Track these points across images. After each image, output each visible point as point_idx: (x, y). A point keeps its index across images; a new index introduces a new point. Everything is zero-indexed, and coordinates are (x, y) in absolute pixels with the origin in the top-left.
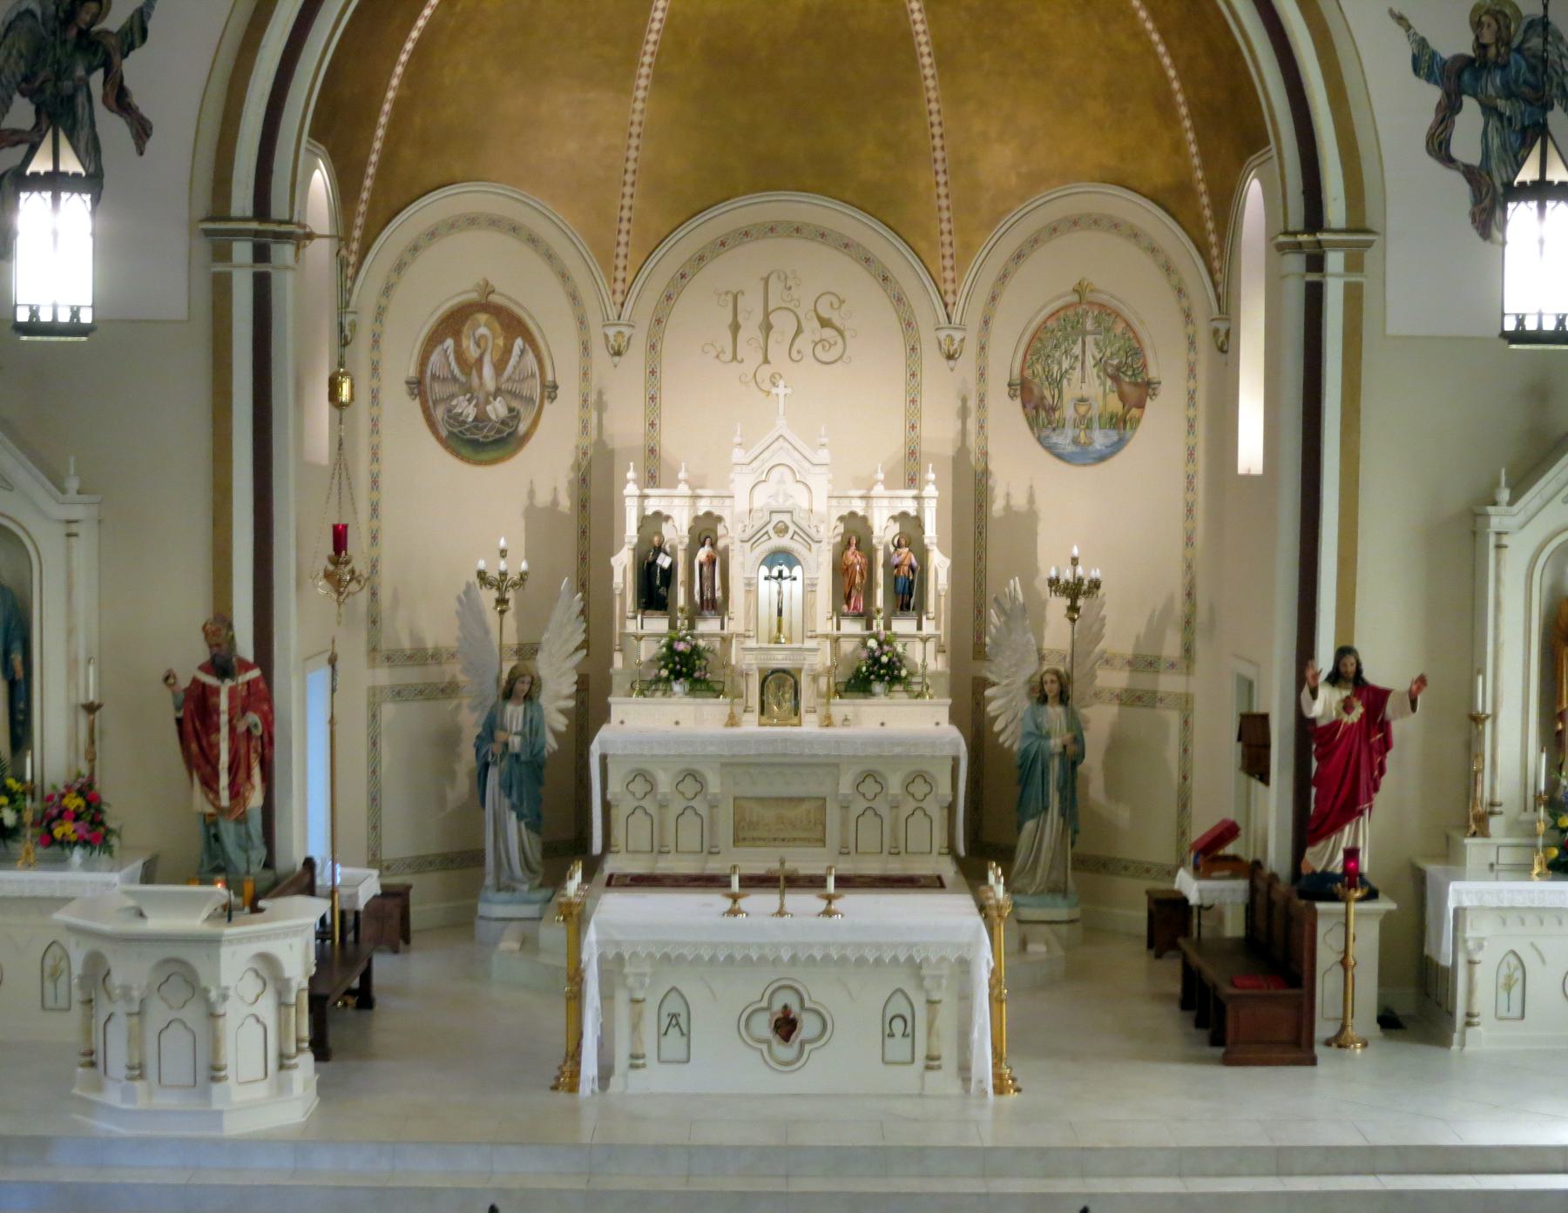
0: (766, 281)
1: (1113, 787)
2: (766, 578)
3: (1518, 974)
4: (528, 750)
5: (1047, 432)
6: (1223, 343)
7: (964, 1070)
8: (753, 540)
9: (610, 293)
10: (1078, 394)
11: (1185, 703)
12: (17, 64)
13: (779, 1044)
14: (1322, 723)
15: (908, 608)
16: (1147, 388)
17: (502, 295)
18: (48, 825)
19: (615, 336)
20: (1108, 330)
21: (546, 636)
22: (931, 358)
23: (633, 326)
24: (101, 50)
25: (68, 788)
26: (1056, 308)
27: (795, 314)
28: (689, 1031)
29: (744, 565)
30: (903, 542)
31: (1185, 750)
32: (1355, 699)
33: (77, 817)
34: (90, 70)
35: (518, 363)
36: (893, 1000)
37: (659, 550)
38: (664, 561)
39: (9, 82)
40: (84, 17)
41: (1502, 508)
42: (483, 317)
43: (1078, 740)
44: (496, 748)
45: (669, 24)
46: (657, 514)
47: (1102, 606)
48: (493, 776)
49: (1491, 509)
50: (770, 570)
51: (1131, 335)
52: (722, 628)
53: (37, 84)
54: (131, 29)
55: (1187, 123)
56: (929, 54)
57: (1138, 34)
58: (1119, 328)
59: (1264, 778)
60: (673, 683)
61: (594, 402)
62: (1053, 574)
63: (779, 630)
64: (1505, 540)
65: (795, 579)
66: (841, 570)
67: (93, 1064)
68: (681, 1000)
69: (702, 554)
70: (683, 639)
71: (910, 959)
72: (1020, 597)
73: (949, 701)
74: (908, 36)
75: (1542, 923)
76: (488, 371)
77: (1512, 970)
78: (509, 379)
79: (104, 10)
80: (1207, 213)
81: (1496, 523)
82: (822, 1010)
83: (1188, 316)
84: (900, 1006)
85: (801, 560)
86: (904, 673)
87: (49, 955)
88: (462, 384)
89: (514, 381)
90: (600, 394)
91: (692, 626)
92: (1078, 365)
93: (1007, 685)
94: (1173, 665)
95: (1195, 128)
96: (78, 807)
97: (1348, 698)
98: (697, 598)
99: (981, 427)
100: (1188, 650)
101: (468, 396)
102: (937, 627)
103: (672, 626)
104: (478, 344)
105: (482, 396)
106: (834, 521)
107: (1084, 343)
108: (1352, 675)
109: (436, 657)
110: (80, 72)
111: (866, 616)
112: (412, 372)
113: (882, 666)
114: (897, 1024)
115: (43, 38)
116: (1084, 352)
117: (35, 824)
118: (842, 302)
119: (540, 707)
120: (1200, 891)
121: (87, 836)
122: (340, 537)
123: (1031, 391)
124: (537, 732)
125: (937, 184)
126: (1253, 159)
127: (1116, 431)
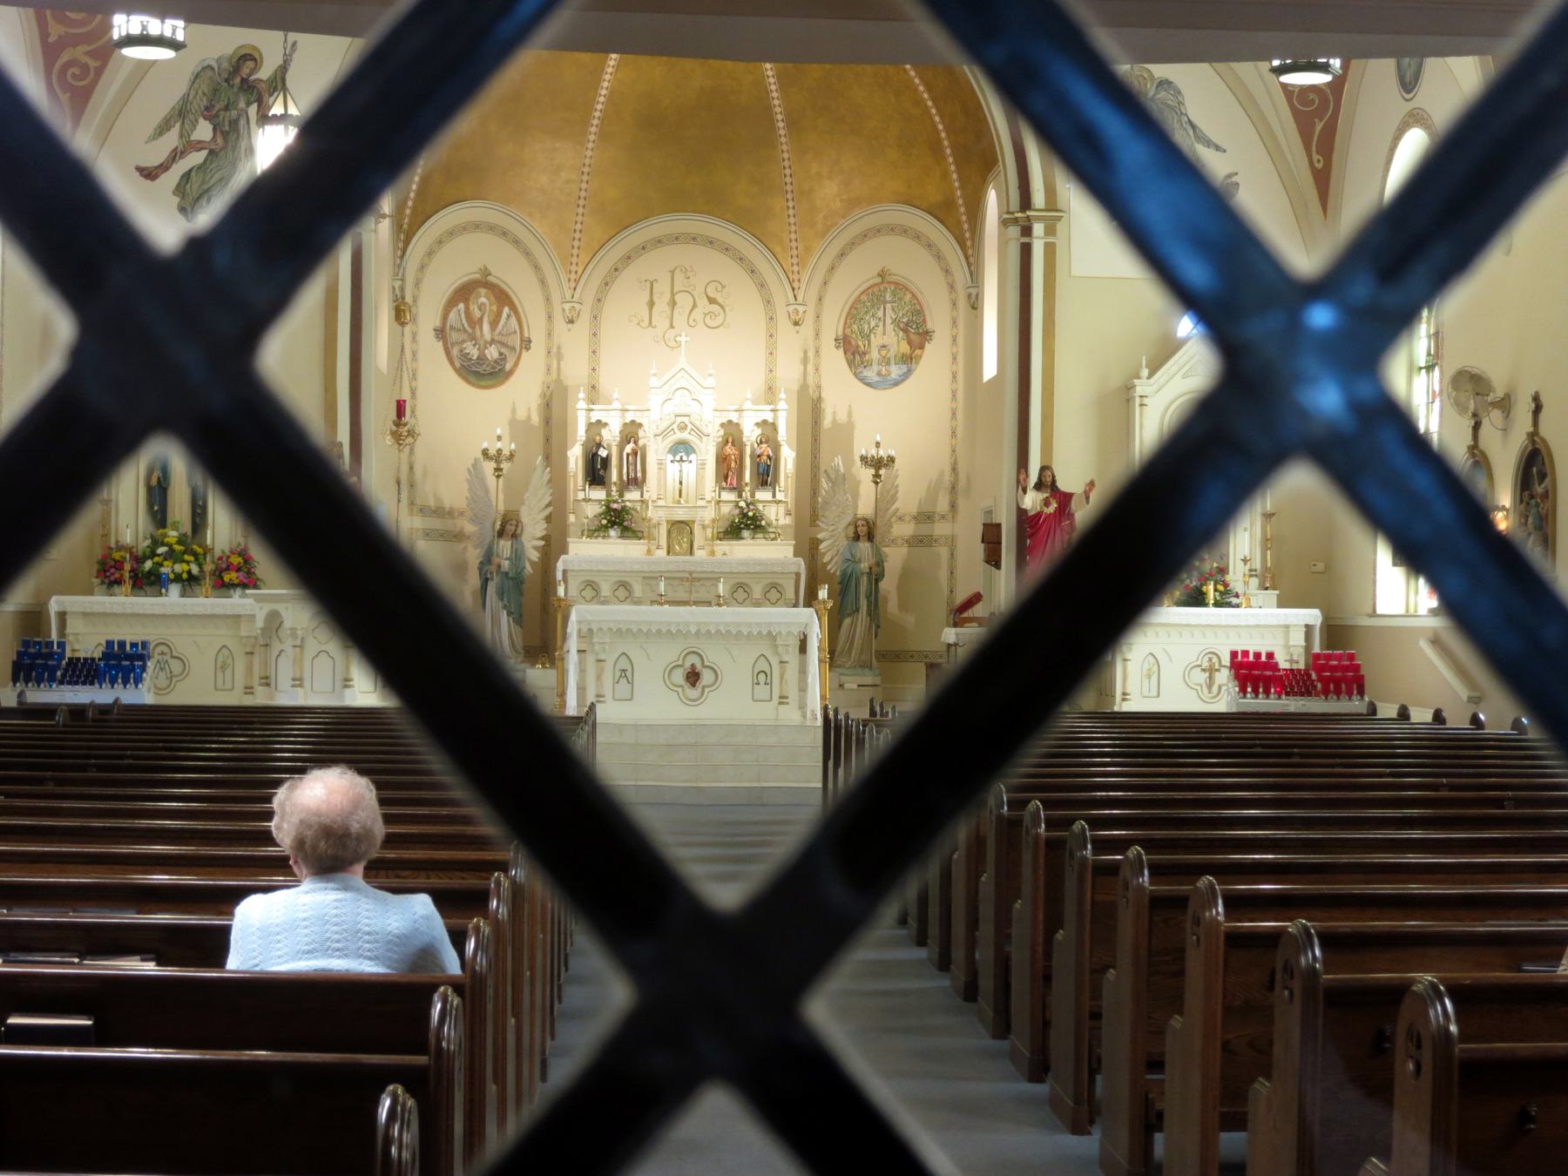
0: (673, 272)
1: (903, 606)
2: (672, 461)
3: (1155, 668)
4: (514, 571)
5: (860, 369)
6: (974, 303)
7: (802, 706)
8: (663, 434)
9: (567, 282)
10: (881, 343)
11: (952, 541)
12: (201, 100)
13: (689, 688)
14: (1031, 513)
15: (766, 484)
16: (926, 335)
17: (496, 277)
18: (220, 574)
19: (570, 310)
20: (900, 299)
21: (527, 495)
22: (784, 324)
23: (581, 304)
24: (255, 91)
25: (232, 552)
26: (866, 287)
27: (692, 295)
28: (633, 680)
29: (656, 451)
30: (763, 440)
31: (952, 573)
32: (1051, 499)
33: (238, 570)
34: (249, 104)
35: (506, 323)
36: (759, 662)
37: (599, 445)
38: (603, 453)
39: (196, 111)
40: (245, 71)
41: (1144, 380)
42: (483, 291)
43: (880, 563)
44: (493, 568)
45: (610, 98)
46: (599, 422)
47: (897, 477)
48: (492, 588)
49: (1136, 381)
50: (674, 456)
51: (916, 302)
52: (642, 496)
53: (214, 112)
54: (275, 78)
55: (951, 160)
56: (783, 120)
57: (919, 102)
58: (908, 297)
59: (998, 565)
60: (610, 530)
61: (554, 354)
62: (864, 452)
63: (680, 496)
64: (1145, 401)
65: (691, 462)
66: (722, 460)
67: (268, 685)
68: (628, 661)
69: (629, 448)
70: (615, 502)
71: (770, 633)
72: (842, 469)
73: (794, 542)
74: (769, 109)
75: (1169, 636)
76: (486, 327)
77: (1151, 665)
78: (500, 333)
79: (259, 63)
80: (964, 218)
81: (1139, 391)
82: (715, 667)
83: (952, 287)
84: (764, 666)
85: (697, 450)
86: (763, 523)
87: (220, 655)
88: (469, 334)
89: (503, 335)
90: (559, 348)
91: (621, 495)
92: (881, 324)
93: (833, 531)
94: (943, 517)
95: (956, 163)
96: (240, 563)
97: (1047, 498)
98: (625, 477)
99: (817, 369)
100: (953, 506)
101: (474, 342)
102: (786, 497)
103: (609, 494)
104: (480, 309)
105: (482, 342)
106: (717, 427)
107: (885, 309)
108: (1049, 484)
109: (450, 513)
110: (242, 105)
111: (739, 490)
112: (438, 323)
113: (749, 518)
114: (762, 676)
115: (218, 83)
116: (885, 315)
117: (213, 574)
118: (724, 287)
119: (522, 543)
120: (957, 634)
121: (245, 581)
122: (400, 407)
123: (850, 343)
124: (520, 559)
125: (788, 207)
126: (991, 177)
127: (905, 366)
